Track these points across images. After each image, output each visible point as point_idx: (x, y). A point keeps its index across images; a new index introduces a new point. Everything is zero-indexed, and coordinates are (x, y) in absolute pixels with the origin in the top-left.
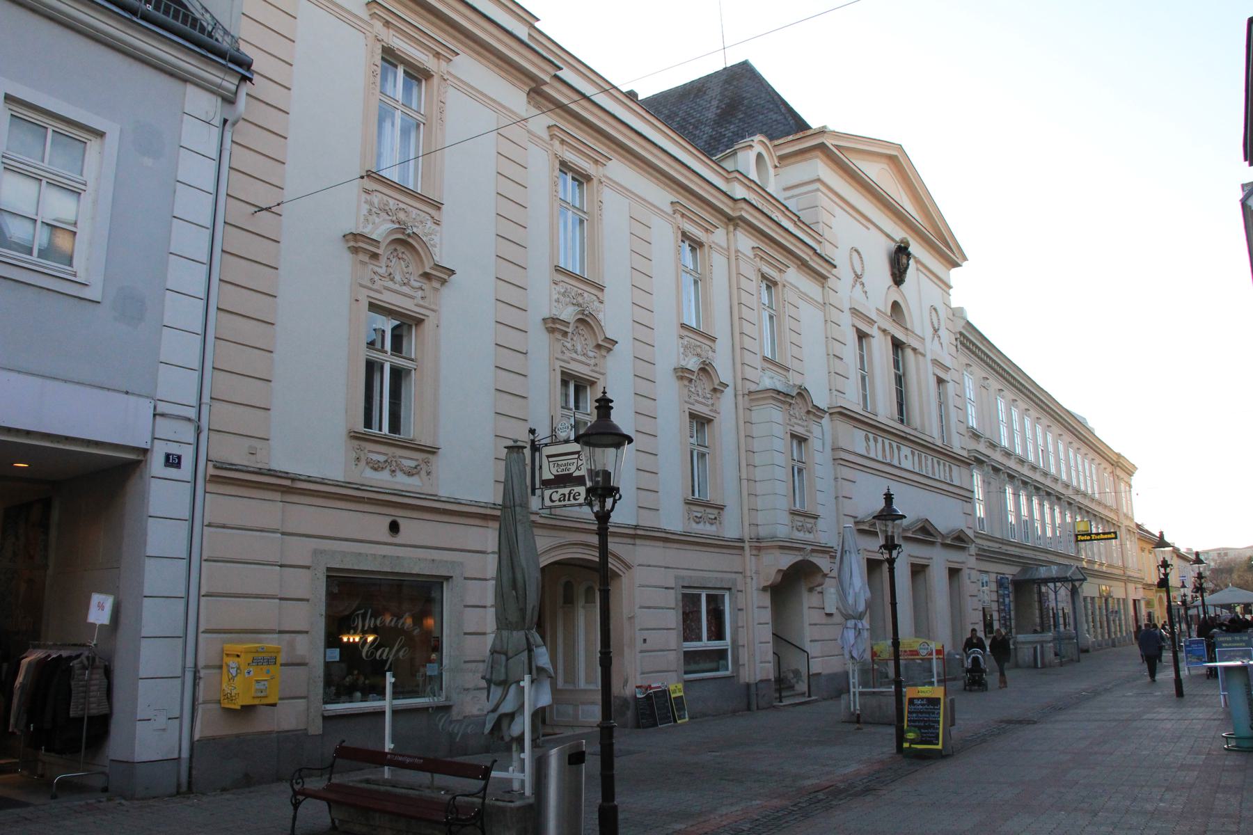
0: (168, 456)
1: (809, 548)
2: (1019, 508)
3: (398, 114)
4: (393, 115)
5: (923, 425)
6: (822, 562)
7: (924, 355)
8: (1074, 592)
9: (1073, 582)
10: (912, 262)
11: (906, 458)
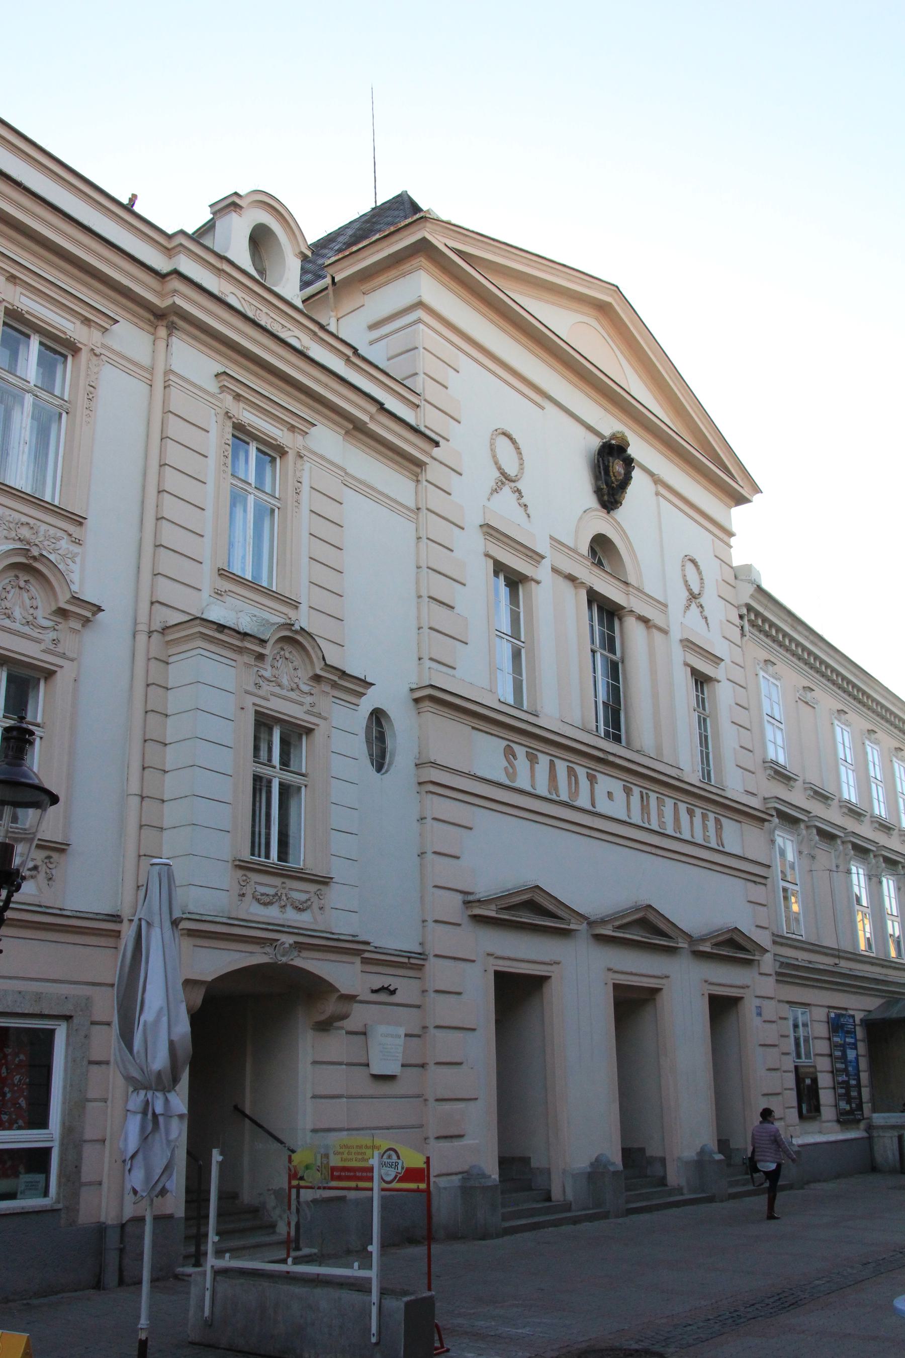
1: (289, 940)
3: (251, 499)
4: (246, 500)
5: (659, 748)
7: (665, 632)
10: (636, 474)
11: (610, 796)
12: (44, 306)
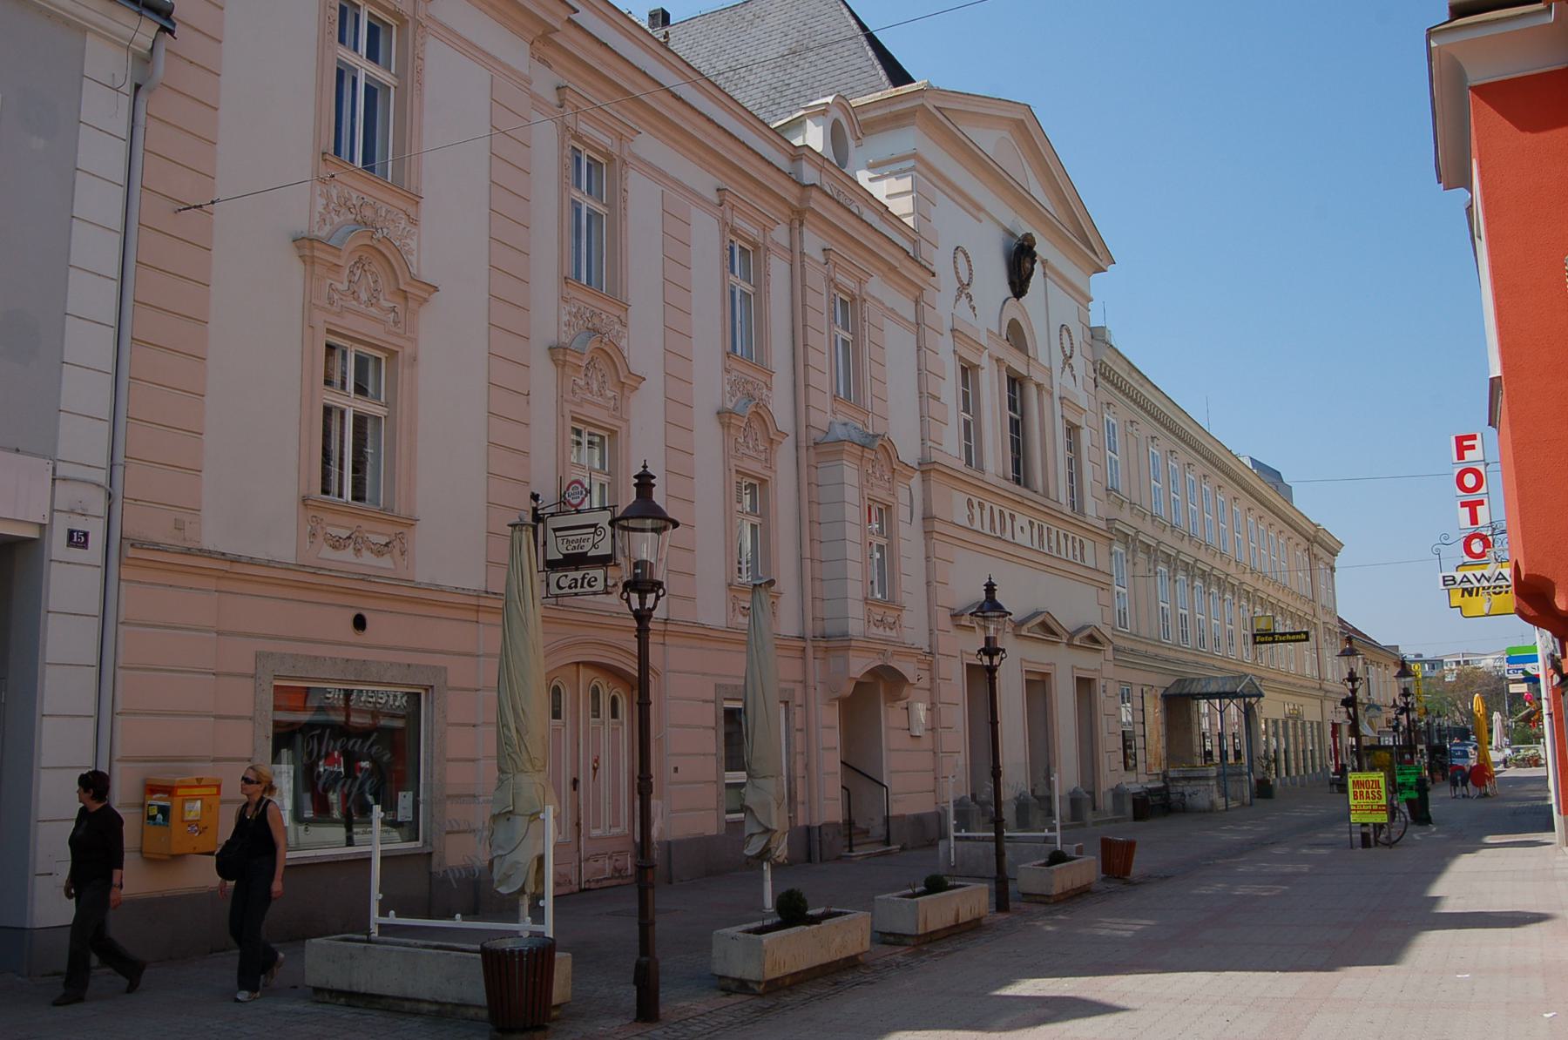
0: (71, 533)
2: (1176, 599)
6: (907, 668)
8: (1249, 714)
9: (1247, 695)
12: (1042, 430)
